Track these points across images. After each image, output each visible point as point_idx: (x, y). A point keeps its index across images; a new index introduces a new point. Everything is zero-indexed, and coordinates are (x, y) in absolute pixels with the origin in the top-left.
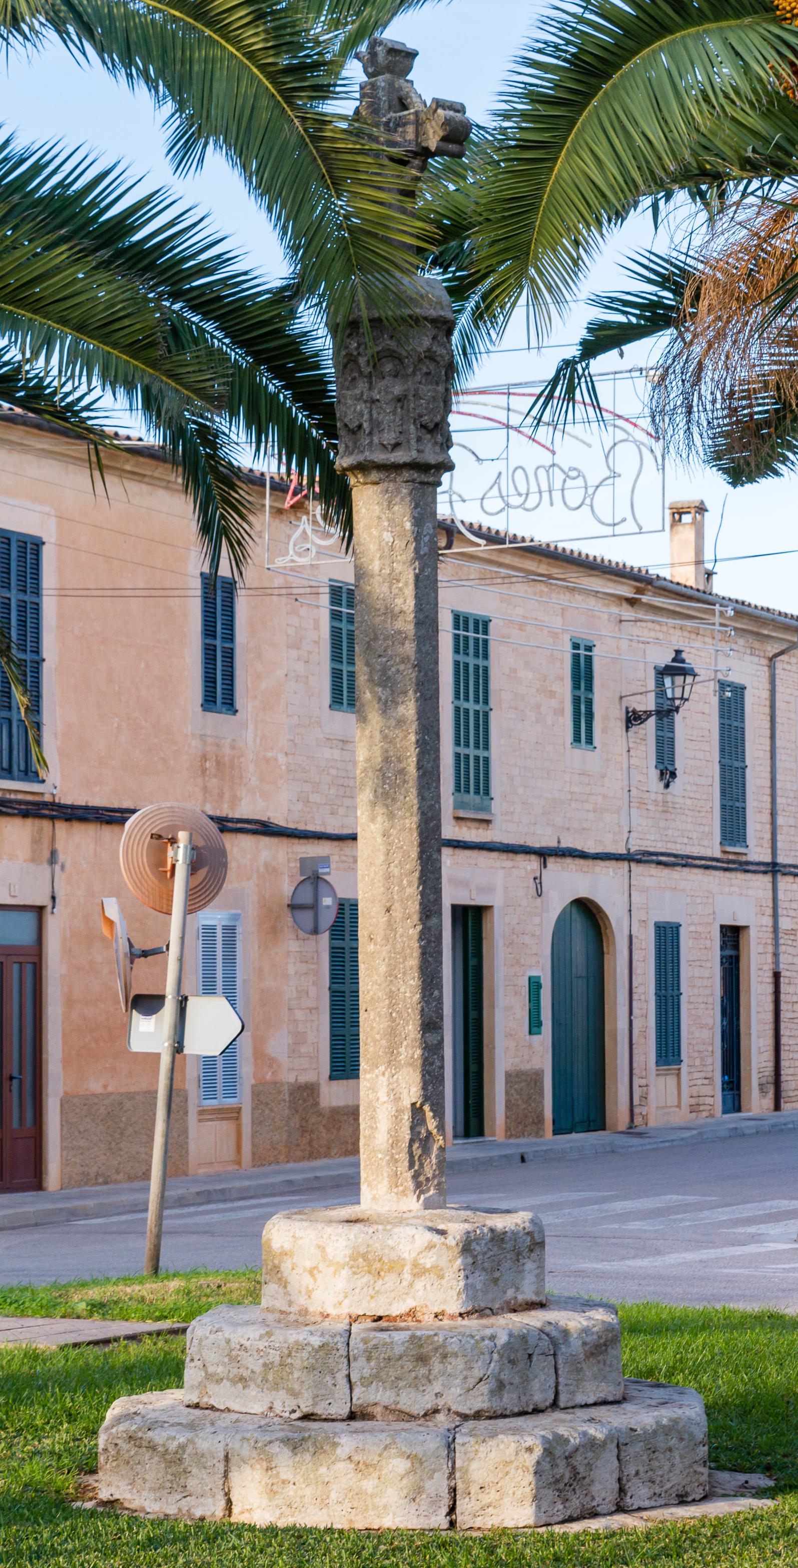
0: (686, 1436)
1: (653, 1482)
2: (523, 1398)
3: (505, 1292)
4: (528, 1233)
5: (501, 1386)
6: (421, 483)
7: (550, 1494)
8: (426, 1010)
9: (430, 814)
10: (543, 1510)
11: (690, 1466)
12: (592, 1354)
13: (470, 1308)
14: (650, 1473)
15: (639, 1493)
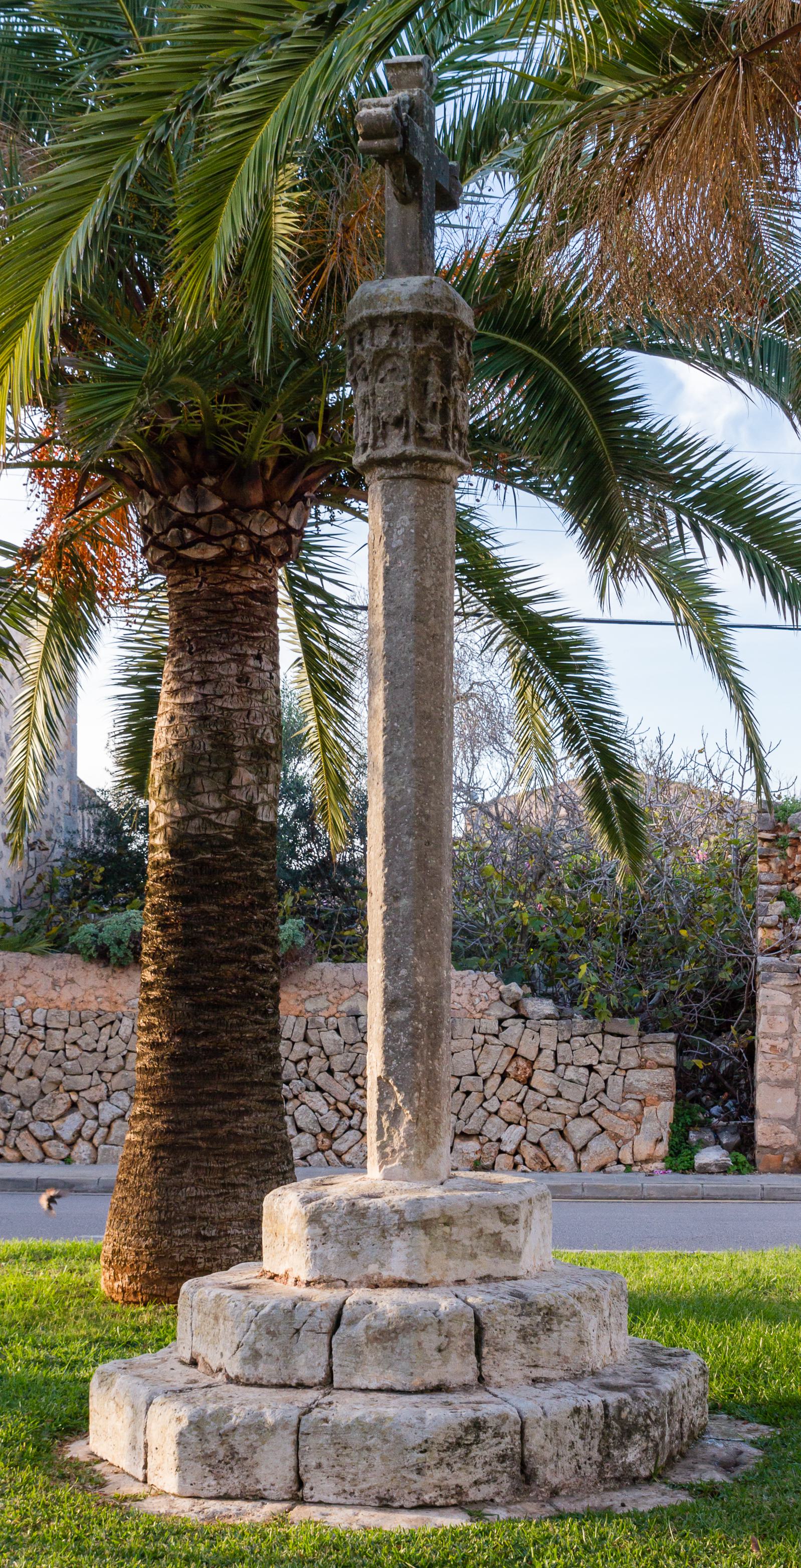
0: (392, 1438)
1: (343, 1479)
2: (283, 1371)
3: (366, 1267)
4: (396, 1212)
5: (255, 1356)
6: (392, 478)
7: (198, 1468)
8: (390, 988)
9: (399, 799)
10: (189, 1481)
11: (396, 1471)
12: (376, 1339)
13: (316, 1277)
14: (337, 1468)
15: (320, 1485)
